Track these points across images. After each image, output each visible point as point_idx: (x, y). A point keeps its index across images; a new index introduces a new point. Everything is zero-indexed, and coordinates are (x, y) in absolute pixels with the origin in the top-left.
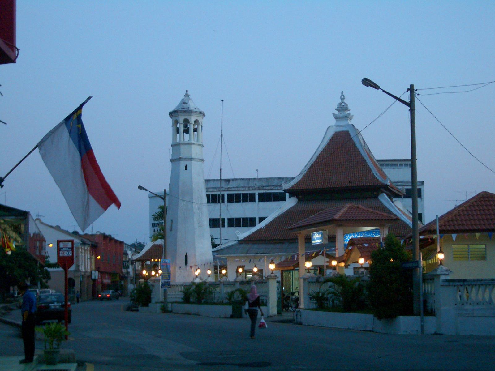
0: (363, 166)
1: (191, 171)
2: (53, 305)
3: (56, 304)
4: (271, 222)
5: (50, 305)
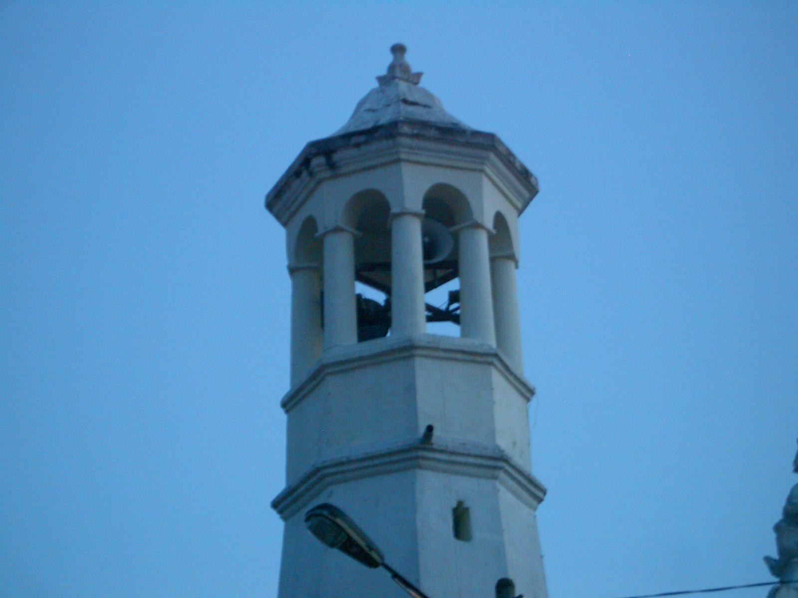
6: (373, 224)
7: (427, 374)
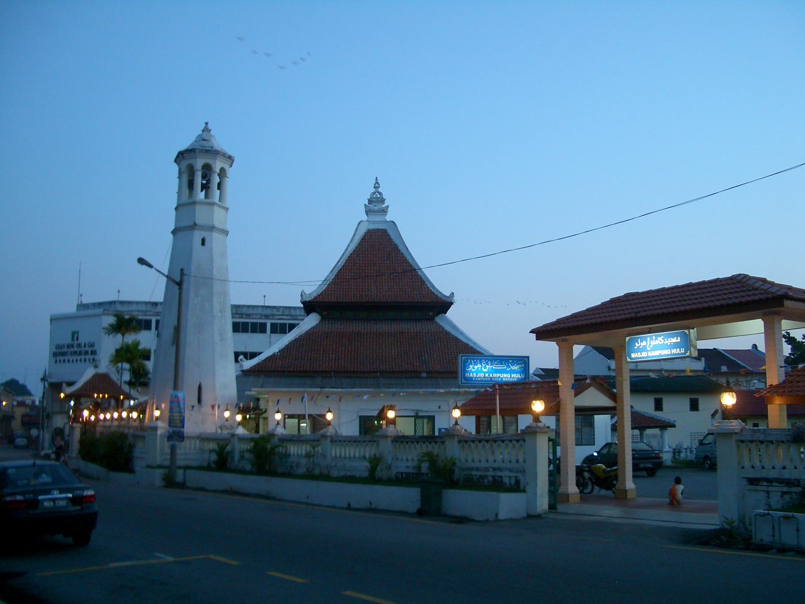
0: (412, 275)
1: (211, 249)
2: (50, 500)
3: (56, 494)
4: (287, 346)
5: (40, 497)
6: (191, 170)
7: (198, 208)
